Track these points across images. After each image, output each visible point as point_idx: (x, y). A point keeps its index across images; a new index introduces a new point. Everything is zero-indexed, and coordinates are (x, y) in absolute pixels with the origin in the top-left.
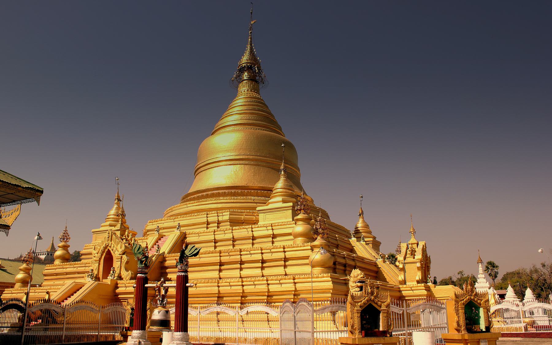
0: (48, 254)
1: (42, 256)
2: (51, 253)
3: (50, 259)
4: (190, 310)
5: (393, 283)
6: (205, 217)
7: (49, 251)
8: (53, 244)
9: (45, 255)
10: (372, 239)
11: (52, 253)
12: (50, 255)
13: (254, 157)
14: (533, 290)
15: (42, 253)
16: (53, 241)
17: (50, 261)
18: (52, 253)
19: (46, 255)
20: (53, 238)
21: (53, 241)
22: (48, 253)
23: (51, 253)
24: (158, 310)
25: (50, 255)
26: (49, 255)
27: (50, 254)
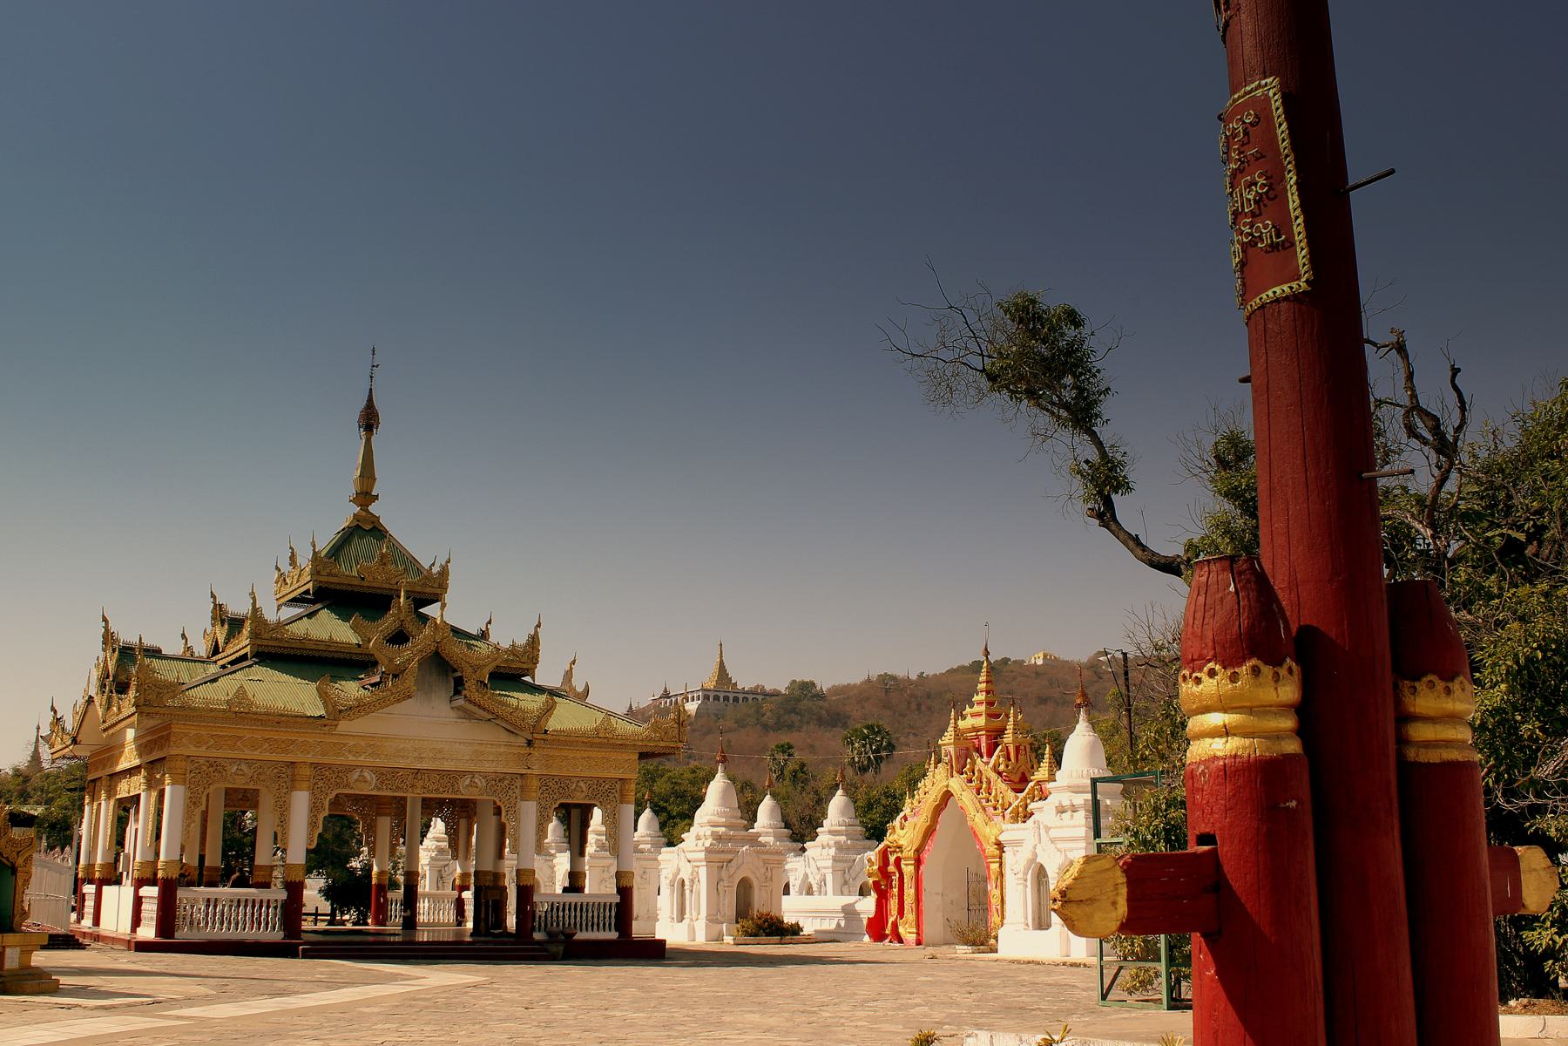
0: (706, 697)
1: (690, 703)
2: (726, 694)
3: (715, 711)
4: (1192, 1036)
5: (387, 711)
6: (1080, 849)
7: (712, 687)
8: (722, 664)
9: (699, 699)
10: (551, 826)
11: (717, 693)
12: (721, 699)
13: (1030, 872)
14: (1106, 735)
15: (690, 696)
16: (721, 657)
17: (713, 717)
18: (717, 693)
19: (700, 702)
20: (721, 645)
21: (721, 657)
22: (707, 693)
23: (726, 694)
24: (1258, 664)
25: (721, 699)
26: (709, 699)
27: (712, 695)
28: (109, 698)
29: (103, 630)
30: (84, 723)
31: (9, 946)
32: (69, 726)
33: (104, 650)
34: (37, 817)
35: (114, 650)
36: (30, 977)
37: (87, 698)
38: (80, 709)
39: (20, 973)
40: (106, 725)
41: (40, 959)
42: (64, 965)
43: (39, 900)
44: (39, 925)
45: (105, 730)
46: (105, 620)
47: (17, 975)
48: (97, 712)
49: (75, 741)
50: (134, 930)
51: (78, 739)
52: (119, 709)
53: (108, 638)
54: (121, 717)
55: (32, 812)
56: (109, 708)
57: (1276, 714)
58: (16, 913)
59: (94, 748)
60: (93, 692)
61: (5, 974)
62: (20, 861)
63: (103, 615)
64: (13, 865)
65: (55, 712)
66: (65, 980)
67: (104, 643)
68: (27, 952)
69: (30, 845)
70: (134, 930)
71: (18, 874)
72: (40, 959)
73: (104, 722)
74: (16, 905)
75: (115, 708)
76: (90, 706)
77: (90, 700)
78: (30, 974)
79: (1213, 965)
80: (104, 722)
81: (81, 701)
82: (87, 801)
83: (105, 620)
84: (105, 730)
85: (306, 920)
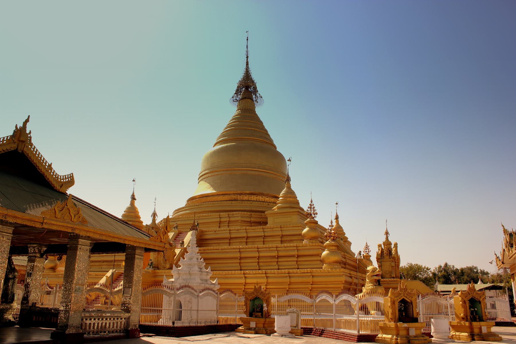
28: (509, 249)
29: (503, 229)
30: (504, 258)
31: (483, 326)
32: (501, 258)
33: (505, 235)
34: (502, 287)
35: (508, 235)
36: (492, 336)
37: (503, 250)
38: (502, 253)
39: (488, 334)
40: (510, 257)
41: (495, 329)
42: (509, 332)
43: (502, 311)
44: (503, 319)
45: (510, 258)
46: (503, 226)
47: (487, 335)
48: (506, 254)
49: (503, 263)
50: (45, 258)
51: (504, 262)
52: (512, 251)
53: (505, 231)
54: (513, 254)
55: (501, 285)
56: (509, 252)
57: (206, 231)
58: (483, 315)
59: (510, 264)
60: (504, 247)
61: (483, 334)
62: (481, 300)
63: (502, 225)
64: (479, 301)
65: (496, 255)
66: (503, 337)
67: (504, 233)
68: (489, 327)
69: (483, 294)
70: (45, 258)
71: (481, 303)
72: (495, 329)
73: (509, 256)
74: (483, 313)
75: (511, 252)
76: (505, 252)
77: (504, 250)
78: (491, 335)
79: (77, 254)
80: (509, 256)
81: (502, 251)
82: (512, 281)
83: (503, 226)
84: (510, 258)
85: (393, 290)
